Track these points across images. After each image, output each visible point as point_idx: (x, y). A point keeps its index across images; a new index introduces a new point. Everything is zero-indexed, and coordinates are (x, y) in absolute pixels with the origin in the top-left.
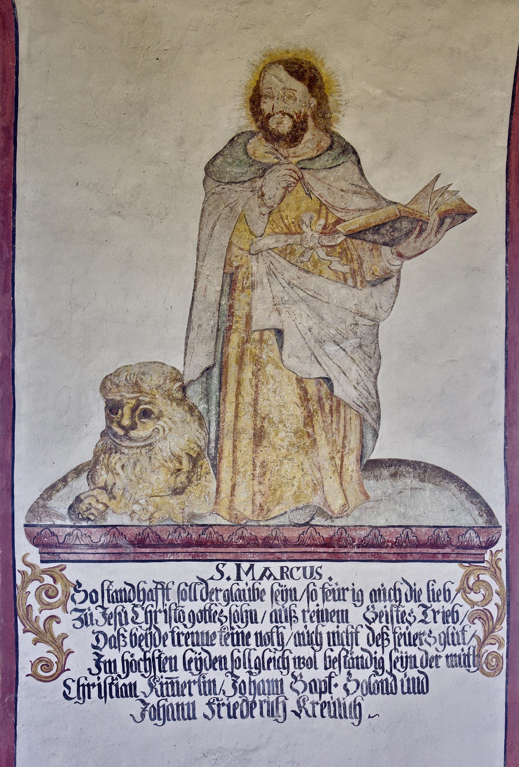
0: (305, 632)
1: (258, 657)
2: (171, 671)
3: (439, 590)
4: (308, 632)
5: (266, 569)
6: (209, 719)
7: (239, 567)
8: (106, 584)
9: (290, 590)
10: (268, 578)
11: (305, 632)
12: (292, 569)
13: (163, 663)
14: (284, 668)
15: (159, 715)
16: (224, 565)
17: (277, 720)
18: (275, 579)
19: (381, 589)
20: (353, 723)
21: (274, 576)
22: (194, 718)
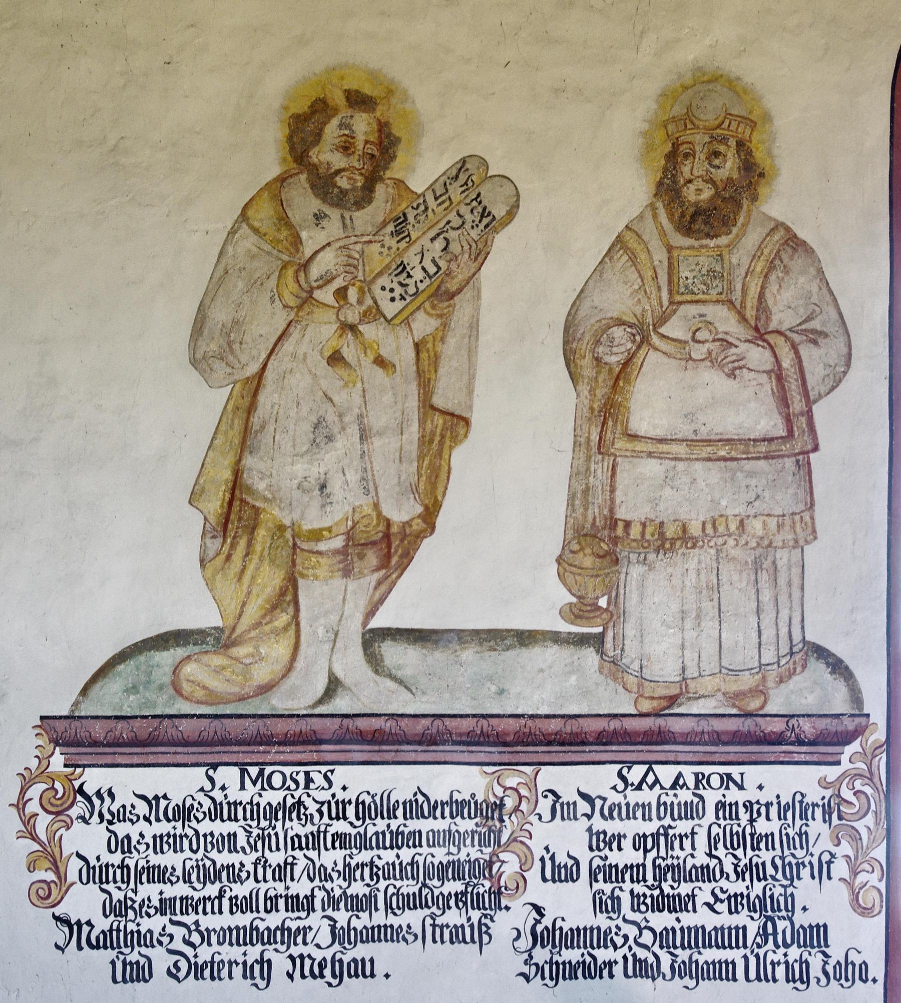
0: (397, 862)
1: (758, 896)
2: (182, 914)
3: (788, 803)
4: (401, 864)
5: (680, 775)
6: (179, 982)
7: (243, 772)
8: (798, 797)
9: (568, 804)
10: (651, 787)
11: (397, 862)
12: (709, 776)
13: (685, 901)
14: (613, 911)
15: (691, 971)
16: (629, 768)
17: (256, 985)
18: (662, 788)
19: (413, 799)
20: (687, 987)
21: (661, 785)
22: (372, 975)
